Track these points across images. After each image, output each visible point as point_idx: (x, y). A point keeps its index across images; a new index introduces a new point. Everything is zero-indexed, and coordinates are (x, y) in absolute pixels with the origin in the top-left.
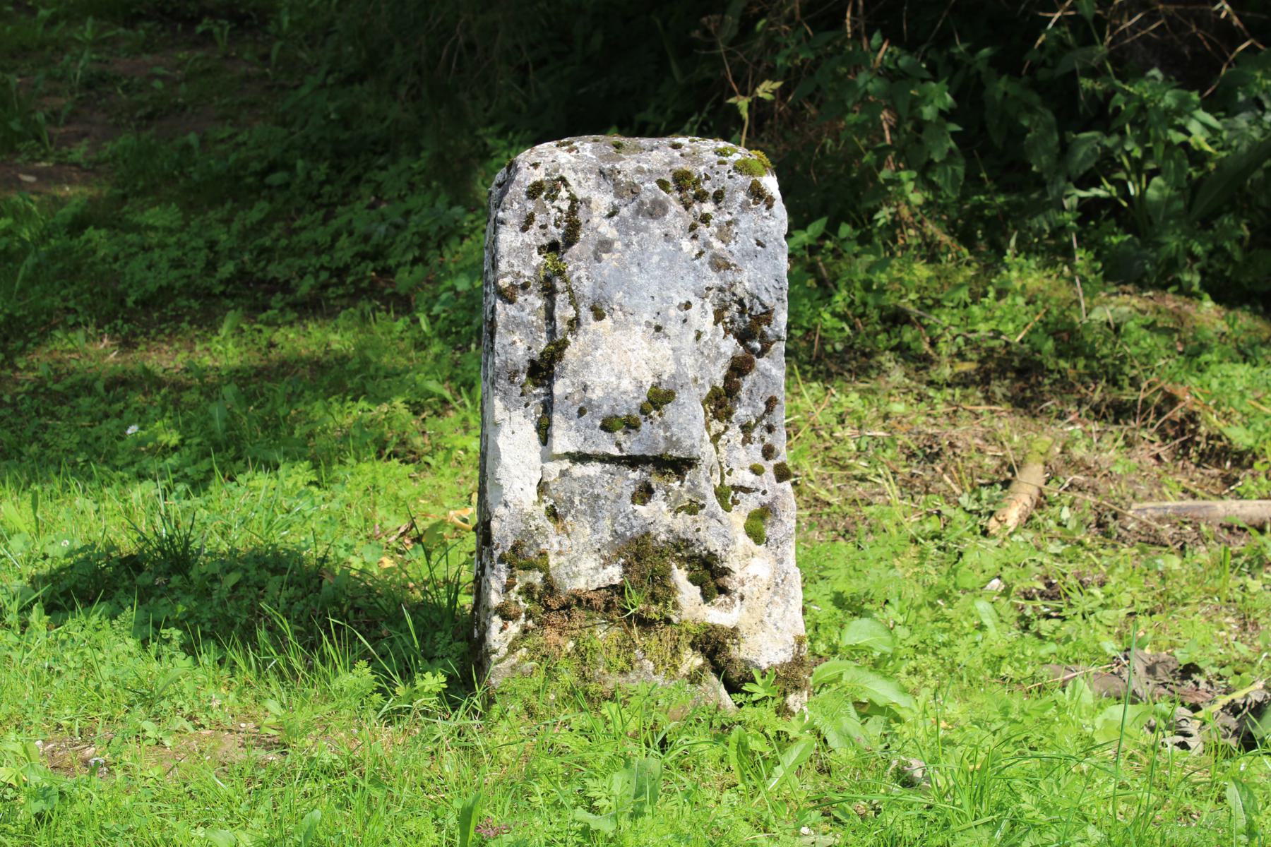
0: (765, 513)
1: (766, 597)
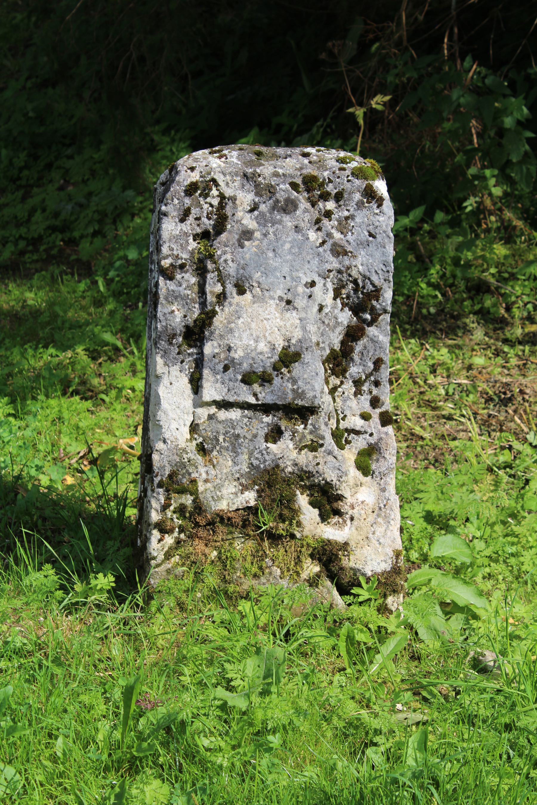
0: (371, 451)
1: (371, 518)
